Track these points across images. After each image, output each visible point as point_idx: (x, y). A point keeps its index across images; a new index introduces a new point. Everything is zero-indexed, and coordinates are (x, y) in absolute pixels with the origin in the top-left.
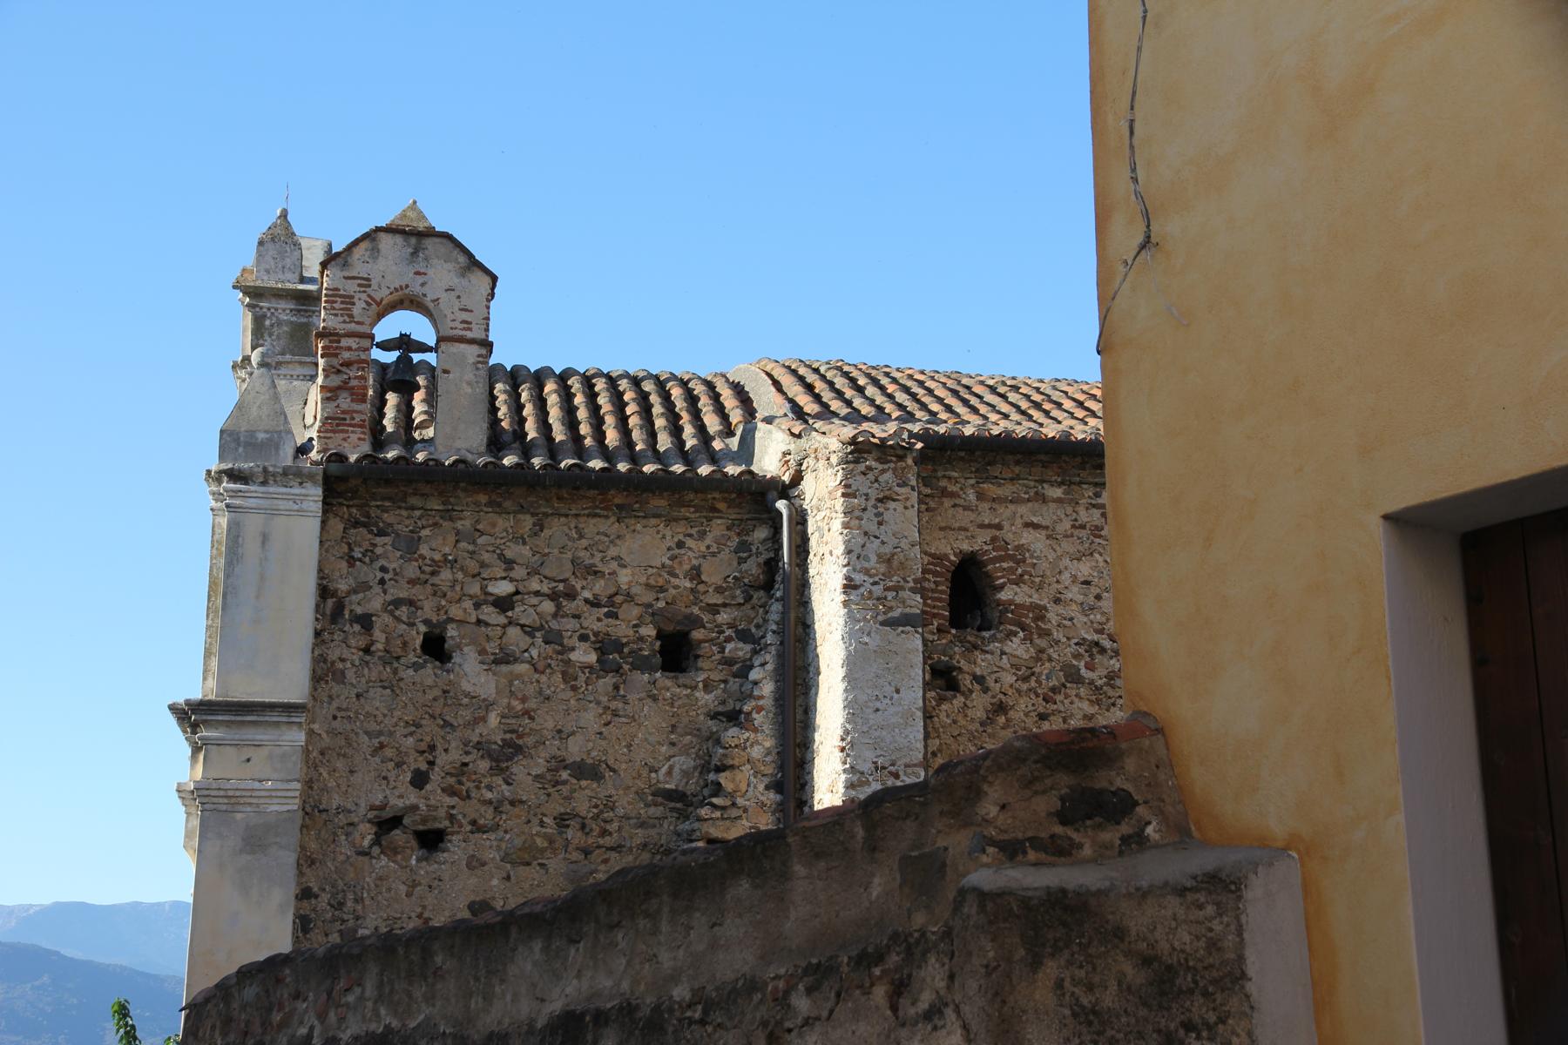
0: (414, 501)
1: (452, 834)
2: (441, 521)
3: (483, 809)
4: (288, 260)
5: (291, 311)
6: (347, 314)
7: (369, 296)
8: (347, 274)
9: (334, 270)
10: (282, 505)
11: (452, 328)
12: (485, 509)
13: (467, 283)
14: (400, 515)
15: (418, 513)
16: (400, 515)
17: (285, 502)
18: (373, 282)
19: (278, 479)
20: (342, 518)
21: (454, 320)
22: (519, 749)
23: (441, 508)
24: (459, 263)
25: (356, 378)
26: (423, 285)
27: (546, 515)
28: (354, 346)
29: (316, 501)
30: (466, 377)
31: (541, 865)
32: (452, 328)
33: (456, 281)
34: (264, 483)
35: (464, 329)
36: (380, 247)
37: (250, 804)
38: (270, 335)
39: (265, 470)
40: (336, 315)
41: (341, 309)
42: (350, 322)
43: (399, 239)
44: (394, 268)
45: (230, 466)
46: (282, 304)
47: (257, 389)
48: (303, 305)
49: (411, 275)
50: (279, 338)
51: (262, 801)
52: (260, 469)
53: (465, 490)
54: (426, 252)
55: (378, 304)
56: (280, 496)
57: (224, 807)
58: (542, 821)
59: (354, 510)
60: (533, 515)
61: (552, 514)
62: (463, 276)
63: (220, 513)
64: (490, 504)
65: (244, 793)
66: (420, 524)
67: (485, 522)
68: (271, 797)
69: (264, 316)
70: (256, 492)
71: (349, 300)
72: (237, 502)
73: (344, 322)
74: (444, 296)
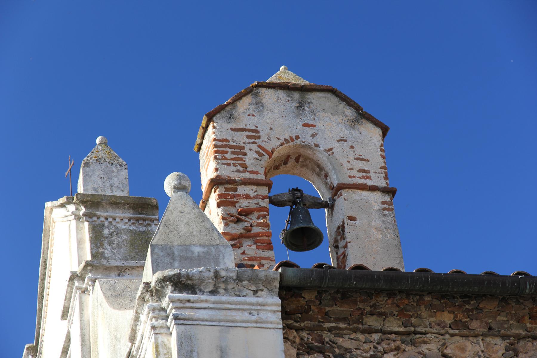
0: (372, 322)
2: (403, 346)
4: (116, 179)
5: (129, 220)
6: (240, 164)
7: (259, 146)
8: (234, 126)
9: (220, 122)
10: (238, 316)
11: (350, 177)
12: (451, 331)
13: (358, 135)
14: (356, 339)
15: (376, 337)
16: (356, 339)
17: (239, 313)
18: (262, 134)
19: (230, 287)
20: (294, 342)
21: (351, 169)
23: (402, 329)
24: (346, 116)
25: (258, 225)
26: (313, 136)
27: (519, 338)
28: (252, 194)
29: (275, 312)
30: (374, 224)
32: (350, 177)
33: (347, 132)
34: (213, 292)
35: (363, 177)
36: (264, 101)
38: (110, 244)
39: (217, 275)
40: (228, 165)
41: (232, 159)
42: (244, 172)
43: (282, 94)
44: (281, 120)
45: (176, 271)
46: (119, 213)
47: (180, 209)
48: (141, 214)
49: (300, 127)
50: (119, 246)
52: (211, 274)
53: (430, 306)
54: (311, 106)
55: (270, 154)
56: (233, 306)
59: (305, 334)
60: (504, 337)
61: (524, 338)
62: (353, 128)
63: (163, 331)
64: (456, 324)
66: (380, 348)
67: (452, 346)
69: (103, 226)
70: (206, 301)
71: (239, 150)
72: (186, 313)
73: (238, 171)
74: (338, 147)
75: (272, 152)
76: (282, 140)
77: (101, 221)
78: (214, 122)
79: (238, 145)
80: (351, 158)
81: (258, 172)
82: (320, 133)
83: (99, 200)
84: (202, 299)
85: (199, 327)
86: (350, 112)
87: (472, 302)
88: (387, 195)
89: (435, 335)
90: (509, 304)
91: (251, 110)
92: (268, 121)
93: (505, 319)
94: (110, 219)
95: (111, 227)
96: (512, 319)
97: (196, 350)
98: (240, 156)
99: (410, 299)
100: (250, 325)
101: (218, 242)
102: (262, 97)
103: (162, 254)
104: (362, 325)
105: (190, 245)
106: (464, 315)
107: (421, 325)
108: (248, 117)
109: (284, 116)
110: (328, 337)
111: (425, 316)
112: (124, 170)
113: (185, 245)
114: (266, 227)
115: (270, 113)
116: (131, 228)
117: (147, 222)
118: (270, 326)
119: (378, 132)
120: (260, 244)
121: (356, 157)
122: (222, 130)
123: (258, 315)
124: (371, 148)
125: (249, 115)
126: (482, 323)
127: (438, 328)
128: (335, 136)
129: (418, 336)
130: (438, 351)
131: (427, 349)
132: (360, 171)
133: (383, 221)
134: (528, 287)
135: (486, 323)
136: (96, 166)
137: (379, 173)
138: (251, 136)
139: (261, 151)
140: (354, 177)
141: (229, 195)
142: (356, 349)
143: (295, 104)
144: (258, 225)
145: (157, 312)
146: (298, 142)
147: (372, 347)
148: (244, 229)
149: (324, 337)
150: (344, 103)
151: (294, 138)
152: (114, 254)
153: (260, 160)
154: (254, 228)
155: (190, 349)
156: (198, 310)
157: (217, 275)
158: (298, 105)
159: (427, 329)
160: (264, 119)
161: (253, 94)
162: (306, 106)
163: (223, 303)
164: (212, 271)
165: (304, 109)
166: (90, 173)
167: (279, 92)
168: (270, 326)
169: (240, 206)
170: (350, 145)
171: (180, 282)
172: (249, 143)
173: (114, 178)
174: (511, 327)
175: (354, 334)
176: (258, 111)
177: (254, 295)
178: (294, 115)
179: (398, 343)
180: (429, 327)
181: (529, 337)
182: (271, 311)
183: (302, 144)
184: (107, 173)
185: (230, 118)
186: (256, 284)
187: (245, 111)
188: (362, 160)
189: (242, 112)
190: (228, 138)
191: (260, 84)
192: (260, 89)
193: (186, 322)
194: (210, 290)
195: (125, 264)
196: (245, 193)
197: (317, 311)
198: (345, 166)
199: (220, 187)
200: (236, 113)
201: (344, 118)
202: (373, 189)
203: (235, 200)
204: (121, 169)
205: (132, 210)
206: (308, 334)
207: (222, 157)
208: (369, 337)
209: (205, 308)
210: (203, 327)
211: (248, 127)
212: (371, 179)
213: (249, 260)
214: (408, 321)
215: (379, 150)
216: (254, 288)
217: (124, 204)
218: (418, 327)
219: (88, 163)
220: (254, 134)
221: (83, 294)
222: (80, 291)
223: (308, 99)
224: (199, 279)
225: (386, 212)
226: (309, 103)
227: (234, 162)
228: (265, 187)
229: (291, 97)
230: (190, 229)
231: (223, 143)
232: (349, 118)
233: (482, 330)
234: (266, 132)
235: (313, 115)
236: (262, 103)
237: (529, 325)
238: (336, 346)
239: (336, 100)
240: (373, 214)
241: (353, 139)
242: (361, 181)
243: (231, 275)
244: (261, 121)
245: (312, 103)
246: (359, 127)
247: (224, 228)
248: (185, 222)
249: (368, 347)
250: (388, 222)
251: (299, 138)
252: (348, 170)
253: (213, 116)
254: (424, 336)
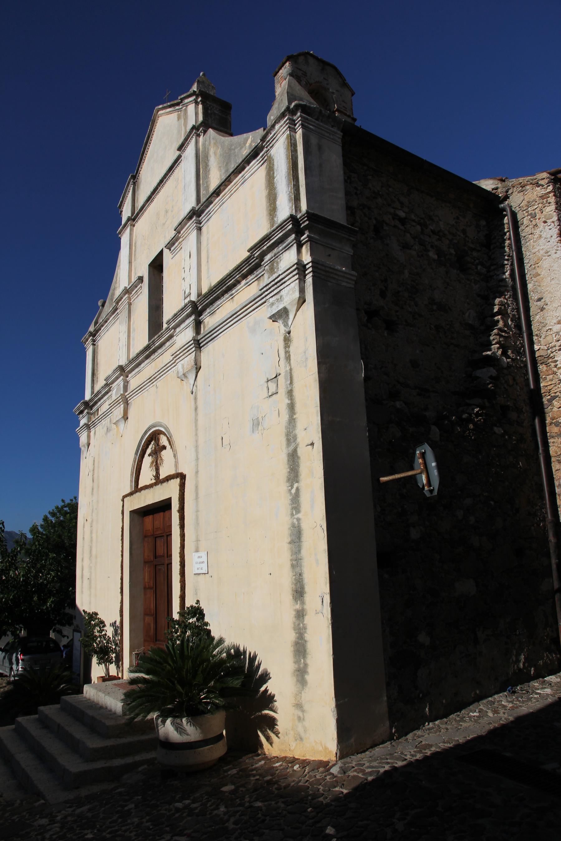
34: (317, 119)
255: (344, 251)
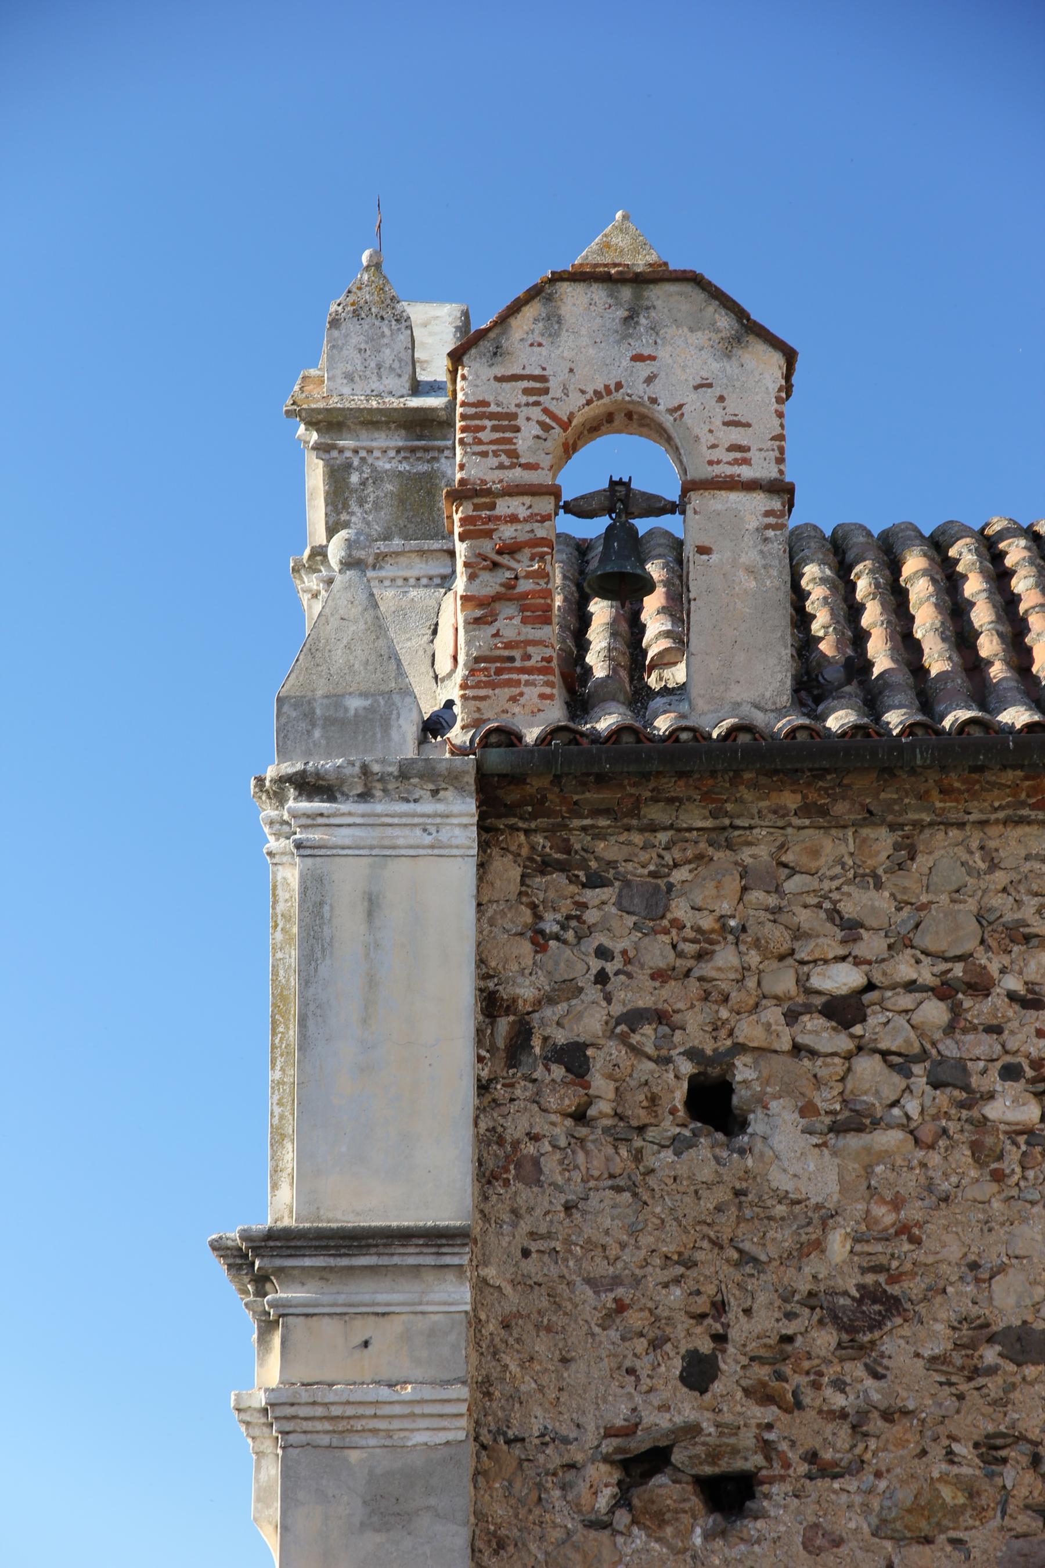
0: (655, 813)
1: (771, 1480)
2: (710, 851)
3: (829, 1429)
4: (388, 351)
5: (398, 451)
7: (546, 411)
8: (500, 371)
9: (476, 365)
11: (711, 463)
12: (797, 821)
14: (629, 843)
15: (663, 837)
16: (629, 843)
17: (406, 831)
18: (552, 384)
20: (519, 855)
21: (714, 446)
22: (893, 1305)
23: (708, 823)
24: (718, 331)
25: (529, 575)
26: (649, 380)
28: (522, 513)
29: (466, 826)
30: (744, 559)
31: (956, 1542)
33: (715, 366)
34: (365, 796)
35: (736, 462)
37: (375, 1431)
38: (361, 502)
39: (365, 770)
40: (484, 454)
41: (492, 442)
43: (598, 293)
44: (592, 351)
45: (299, 766)
47: (341, 612)
49: (626, 362)
50: (377, 506)
51: (396, 1424)
52: (357, 769)
53: (754, 786)
54: (653, 314)
55: (565, 426)
56: (396, 821)
57: (325, 1440)
58: (950, 1452)
60: (893, 827)
61: (931, 824)
62: (728, 355)
63: (285, 859)
64: (805, 810)
65: (360, 1411)
66: (668, 858)
67: (797, 848)
68: (412, 1415)
69: (348, 466)
70: (350, 814)
71: (507, 422)
72: (315, 836)
73: (501, 467)
74: (692, 400)
75: (570, 422)
76: (590, 394)
77: (347, 458)
78: (463, 367)
79: (504, 411)
80: (718, 422)
81: (538, 464)
82: (662, 375)
83: (340, 419)
84: (342, 811)
85: (337, 859)
86: (725, 322)
87: (829, 777)
88: (776, 497)
89: (768, 830)
90: (895, 775)
91: (537, 332)
92: (566, 354)
93: (895, 796)
94: (363, 454)
95: (364, 468)
96: (907, 797)
97: (329, 902)
98: (508, 435)
99: (716, 778)
100: (421, 852)
101: (393, 685)
102: (559, 303)
103: (294, 714)
104: (639, 819)
105: (343, 696)
106: (819, 795)
107: (742, 815)
108: (530, 349)
109: (598, 340)
110: (581, 841)
111: (750, 799)
112: (403, 330)
113: (335, 695)
114: (543, 577)
115: (572, 337)
116: (401, 468)
117: (431, 454)
118: (455, 852)
119: (776, 360)
120: (528, 614)
121: (727, 418)
122: (478, 382)
123: (438, 832)
124: (758, 398)
125: (532, 345)
126: (854, 805)
127: (773, 817)
128: (691, 378)
129: (737, 833)
130: (769, 859)
131: (751, 856)
132: (734, 448)
133: (761, 552)
134: (919, 756)
135: (862, 805)
136: (351, 326)
137: (768, 450)
138: (533, 389)
139: (548, 420)
140: (719, 462)
141: (480, 517)
142: (625, 861)
143: (622, 313)
144: (529, 575)
145: (277, 826)
146: (618, 396)
147: (654, 855)
148: (502, 585)
149: (572, 841)
150: (717, 303)
151: (612, 387)
152: (368, 523)
153: (545, 440)
154: (521, 582)
155: (318, 900)
156: (336, 828)
157: (365, 770)
158: (626, 314)
159: (752, 822)
160: (558, 352)
161: (544, 298)
162: (641, 316)
163: (379, 816)
164: (358, 764)
165: (637, 323)
166: (340, 343)
167: (595, 286)
168: (455, 852)
169: (500, 538)
170: (718, 395)
171: (308, 783)
172: (527, 404)
173: (383, 349)
174: (905, 811)
175: (626, 833)
176: (550, 335)
177: (433, 796)
178: (618, 337)
179: (703, 845)
180: (757, 816)
181: (940, 823)
182: (459, 825)
183: (627, 398)
184: (373, 340)
185: (495, 354)
186: (433, 782)
187: (525, 336)
188: (737, 424)
189: (518, 338)
190: (490, 398)
191: (556, 276)
192: (559, 284)
193: (316, 852)
194: (359, 792)
195: (382, 549)
196: (509, 512)
197: (557, 800)
198: (703, 440)
199: (465, 504)
200: (508, 343)
201: (713, 335)
202: (751, 486)
203: (491, 526)
204: (399, 329)
205: (403, 432)
206: (546, 838)
207: (475, 438)
208: (652, 838)
209: (349, 825)
210: (343, 859)
211: (527, 372)
212: (750, 465)
213: (505, 648)
214: (721, 808)
215: (774, 400)
216: (431, 787)
217: (387, 423)
218: (738, 817)
219: (337, 320)
220: (538, 385)
221: (315, 600)
222: (310, 596)
223: (648, 299)
224: (337, 779)
225: (771, 533)
226: (648, 308)
227: (494, 447)
228: (547, 497)
229: (616, 298)
230: (351, 658)
231: (478, 410)
232: (723, 335)
233: (852, 817)
234: (560, 379)
235: (654, 335)
236: (559, 316)
237: (939, 805)
238: (592, 857)
239: (699, 296)
240: (745, 539)
241: (725, 381)
242: (730, 470)
243: (391, 769)
244: (553, 355)
245: (654, 308)
246: (740, 352)
247: (466, 586)
248: (345, 642)
249: (648, 856)
250: (771, 554)
251: (622, 387)
252: (709, 448)
253: (464, 354)
254: (748, 832)
255: (430, 1308)
